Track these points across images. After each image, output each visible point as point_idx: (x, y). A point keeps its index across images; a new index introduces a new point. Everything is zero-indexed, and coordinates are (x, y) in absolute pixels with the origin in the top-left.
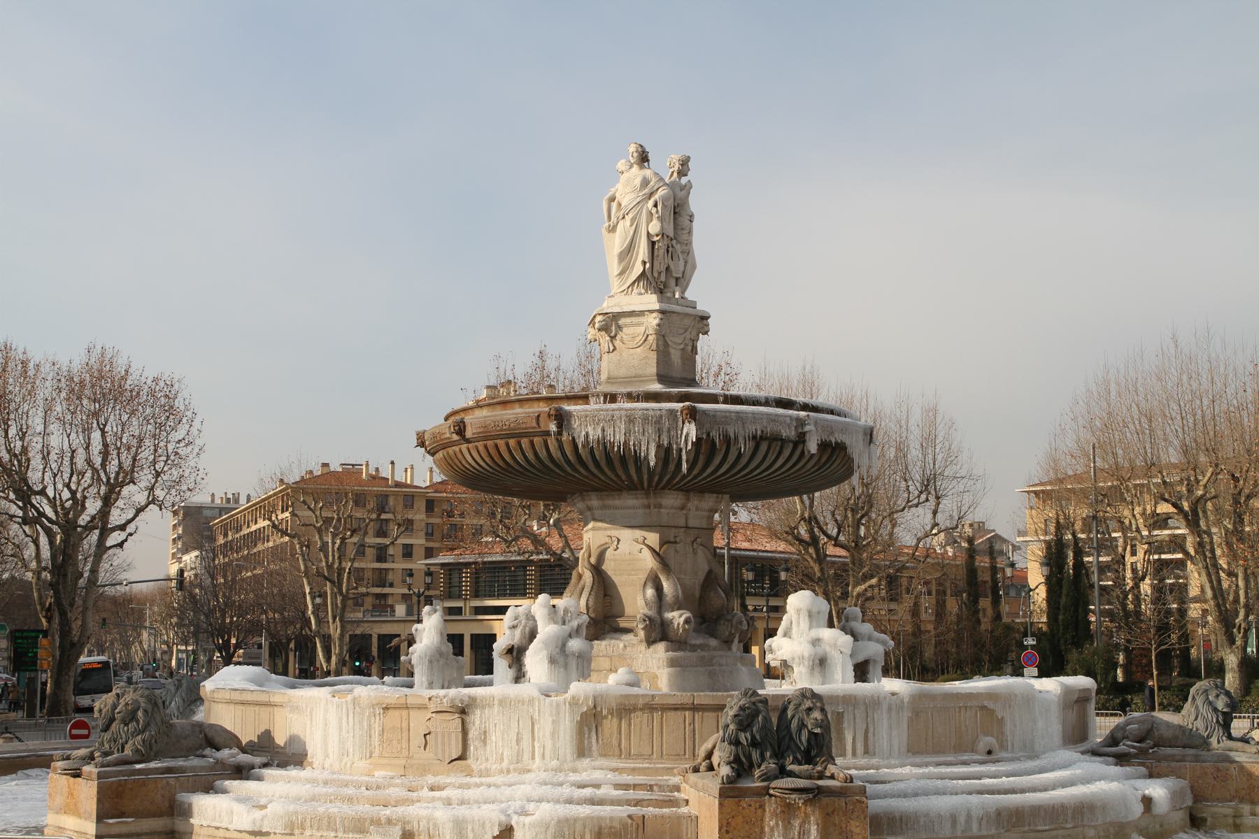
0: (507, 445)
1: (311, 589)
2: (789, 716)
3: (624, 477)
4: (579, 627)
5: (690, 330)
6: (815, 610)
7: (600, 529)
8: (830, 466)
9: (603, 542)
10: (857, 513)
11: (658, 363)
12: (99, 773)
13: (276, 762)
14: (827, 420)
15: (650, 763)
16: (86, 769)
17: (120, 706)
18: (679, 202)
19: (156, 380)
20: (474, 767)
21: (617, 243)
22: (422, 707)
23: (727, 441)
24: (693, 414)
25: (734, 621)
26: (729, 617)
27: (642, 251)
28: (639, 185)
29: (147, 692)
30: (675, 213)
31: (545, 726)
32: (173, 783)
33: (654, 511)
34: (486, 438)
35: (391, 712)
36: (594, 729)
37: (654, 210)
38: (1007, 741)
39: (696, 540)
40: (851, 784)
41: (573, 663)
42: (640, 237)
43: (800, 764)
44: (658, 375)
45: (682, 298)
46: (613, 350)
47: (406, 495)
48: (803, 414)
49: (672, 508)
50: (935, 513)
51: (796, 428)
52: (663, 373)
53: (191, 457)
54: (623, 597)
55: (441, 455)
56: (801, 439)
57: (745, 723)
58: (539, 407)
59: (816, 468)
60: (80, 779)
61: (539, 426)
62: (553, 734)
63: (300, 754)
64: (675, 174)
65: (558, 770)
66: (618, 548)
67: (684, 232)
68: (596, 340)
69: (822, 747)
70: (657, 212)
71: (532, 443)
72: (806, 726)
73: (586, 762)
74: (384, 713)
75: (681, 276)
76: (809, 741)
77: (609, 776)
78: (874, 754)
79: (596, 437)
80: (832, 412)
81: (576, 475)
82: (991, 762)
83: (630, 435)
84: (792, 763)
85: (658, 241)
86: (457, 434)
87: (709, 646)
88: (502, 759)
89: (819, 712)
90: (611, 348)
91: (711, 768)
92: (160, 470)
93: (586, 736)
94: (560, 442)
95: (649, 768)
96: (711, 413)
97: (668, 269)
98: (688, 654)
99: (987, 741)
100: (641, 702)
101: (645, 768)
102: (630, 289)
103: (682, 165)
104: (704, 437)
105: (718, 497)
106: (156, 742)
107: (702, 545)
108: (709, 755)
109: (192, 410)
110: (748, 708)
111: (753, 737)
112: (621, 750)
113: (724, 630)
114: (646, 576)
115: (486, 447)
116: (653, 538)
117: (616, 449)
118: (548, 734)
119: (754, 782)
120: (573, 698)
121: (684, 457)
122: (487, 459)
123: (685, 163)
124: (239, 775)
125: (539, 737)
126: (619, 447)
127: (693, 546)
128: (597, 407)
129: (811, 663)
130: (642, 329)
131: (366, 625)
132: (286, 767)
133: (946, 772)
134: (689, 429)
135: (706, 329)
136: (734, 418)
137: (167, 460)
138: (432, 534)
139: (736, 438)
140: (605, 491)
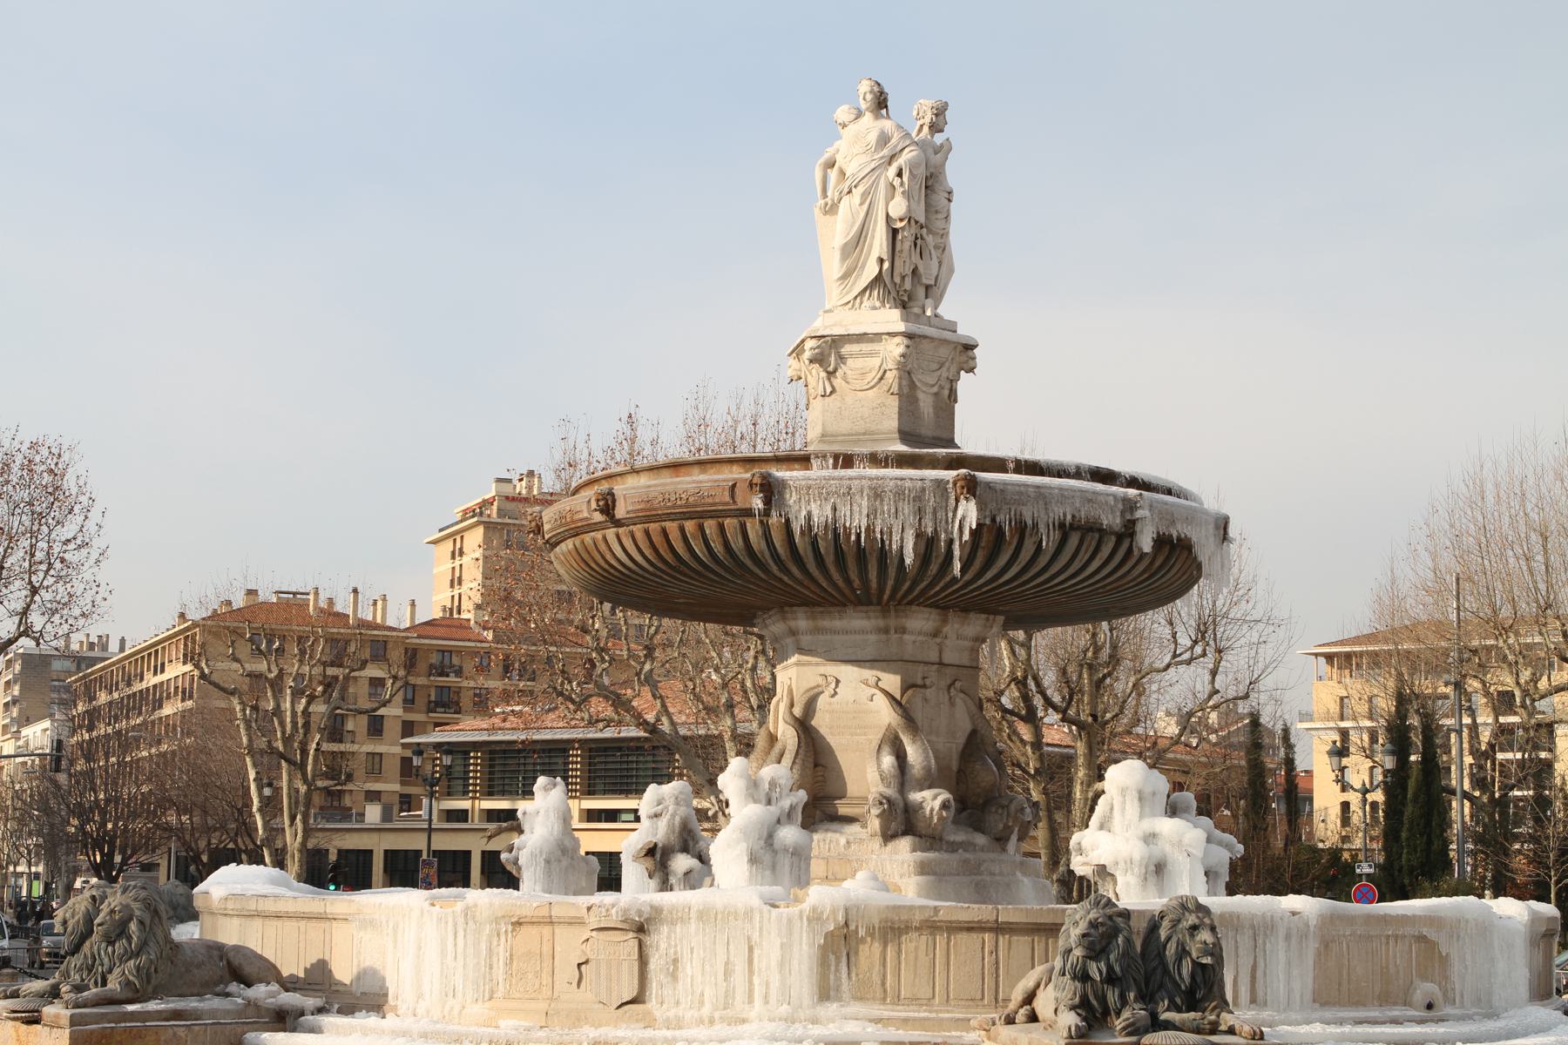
0: (682, 529)
1: (257, 773)
2: (1163, 939)
3: (857, 583)
4: (792, 808)
5: (947, 364)
6: (1148, 790)
7: (809, 664)
8: (1166, 574)
9: (813, 685)
10: (1097, 671)
11: (900, 414)
12: (72, 1016)
13: (336, 1006)
14: (1166, 504)
15: (930, 1012)
16: (49, 1011)
17: (101, 915)
18: (932, 170)
19: (33, 446)
20: (657, 1014)
21: (839, 229)
22: (576, 922)
23: (1021, 529)
24: (971, 487)
25: (1013, 807)
26: (1005, 802)
27: (878, 243)
28: (873, 142)
29: (143, 894)
30: (926, 187)
31: (769, 953)
32: (183, 1035)
33: (894, 637)
34: (648, 519)
35: (525, 931)
36: (844, 959)
37: (897, 182)
38: (1453, 989)
39: (953, 683)
40: (1262, 1042)
41: (785, 862)
42: (876, 221)
43: (1179, 1010)
44: (901, 432)
45: (936, 316)
46: (831, 393)
47: (374, 641)
48: (1132, 492)
49: (920, 633)
50: (1214, 673)
51: (1123, 513)
52: (907, 429)
53: (87, 565)
54: (843, 769)
55: (571, 546)
56: (1129, 530)
57: (1098, 947)
58: (731, 472)
59: (1146, 576)
60: (38, 1027)
61: (734, 502)
62: (782, 964)
63: (374, 994)
64: (926, 129)
65: (791, 1020)
66: (836, 693)
67: (939, 216)
68: (800, 378)
69: (1212, 986)
70: (902, 184)
71: (721, 527)
72: (1189, 954)
73: (833, 1008)
74: (513, 931)
75: (933, 283)
76: (1193, 976)
77: (869, 1030)
78: (1265, 1004)
79: (823, 519)
80: (1169, 492)
81: (786, 579)
82: (1432, 1021)
83: (875, 518)
84: (1168, 1010)
85: (903, 228)
86: (602, 512)
87: (975, 845)
88: (702, 1003)
89: (1209, 933)
90: (829, 390)
91: (1033, 1018)
92: (37, 585)
93: (833, 968)
94: (766, 527)
95: (928, 1019)
96: (998, 487)
97: (915, 272)
98: (946, 856)
99: (1425, 989)
100: (918, 917)
101: (925, 1019)
102: (858, 298)
103: (937, 115)
104: (988, 521)
105: (987, 619)
106: (156, 971)
107: (962, 691)
108: (1029, 998)
109: (88, 495)
110: (1102, 924)
111: (1110, 968)
112: (885, 991)
113: (996, 821)
114: (880, 736)
115: (647, 532)
116: (892, 682)
117: (853, 538)
118: (774, 963)
119: (1115, 1037)
120: (814, 909)
121: (957, 553)
122: (648, 552)
123: (940, 112)
124: (281, 1025)
125: (760, 970)
126: (858, 536)
127: (949, 693)
128: (825, 473)
129: (1144, 871)
130: (876, 362)
131: (320, 834)
132: (353, 1013)
133: (1374, 1033)
134: (966, 510)
135: (971, 363)
136: (1032, 495)
137: (48, 570)
138: (413, 702)
139: (1035, 525)
140: (819, 605)
